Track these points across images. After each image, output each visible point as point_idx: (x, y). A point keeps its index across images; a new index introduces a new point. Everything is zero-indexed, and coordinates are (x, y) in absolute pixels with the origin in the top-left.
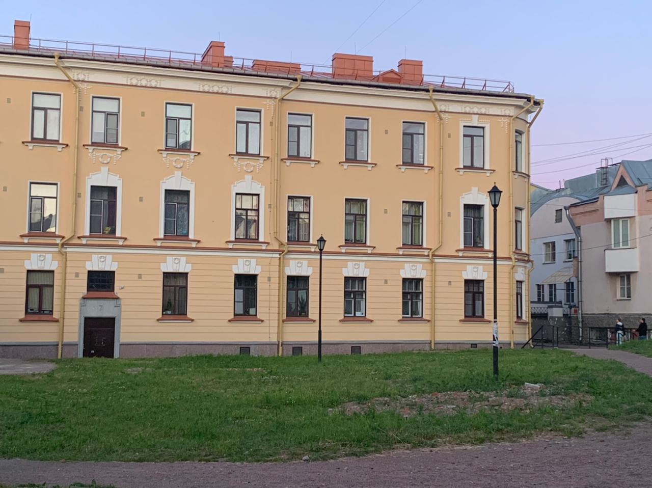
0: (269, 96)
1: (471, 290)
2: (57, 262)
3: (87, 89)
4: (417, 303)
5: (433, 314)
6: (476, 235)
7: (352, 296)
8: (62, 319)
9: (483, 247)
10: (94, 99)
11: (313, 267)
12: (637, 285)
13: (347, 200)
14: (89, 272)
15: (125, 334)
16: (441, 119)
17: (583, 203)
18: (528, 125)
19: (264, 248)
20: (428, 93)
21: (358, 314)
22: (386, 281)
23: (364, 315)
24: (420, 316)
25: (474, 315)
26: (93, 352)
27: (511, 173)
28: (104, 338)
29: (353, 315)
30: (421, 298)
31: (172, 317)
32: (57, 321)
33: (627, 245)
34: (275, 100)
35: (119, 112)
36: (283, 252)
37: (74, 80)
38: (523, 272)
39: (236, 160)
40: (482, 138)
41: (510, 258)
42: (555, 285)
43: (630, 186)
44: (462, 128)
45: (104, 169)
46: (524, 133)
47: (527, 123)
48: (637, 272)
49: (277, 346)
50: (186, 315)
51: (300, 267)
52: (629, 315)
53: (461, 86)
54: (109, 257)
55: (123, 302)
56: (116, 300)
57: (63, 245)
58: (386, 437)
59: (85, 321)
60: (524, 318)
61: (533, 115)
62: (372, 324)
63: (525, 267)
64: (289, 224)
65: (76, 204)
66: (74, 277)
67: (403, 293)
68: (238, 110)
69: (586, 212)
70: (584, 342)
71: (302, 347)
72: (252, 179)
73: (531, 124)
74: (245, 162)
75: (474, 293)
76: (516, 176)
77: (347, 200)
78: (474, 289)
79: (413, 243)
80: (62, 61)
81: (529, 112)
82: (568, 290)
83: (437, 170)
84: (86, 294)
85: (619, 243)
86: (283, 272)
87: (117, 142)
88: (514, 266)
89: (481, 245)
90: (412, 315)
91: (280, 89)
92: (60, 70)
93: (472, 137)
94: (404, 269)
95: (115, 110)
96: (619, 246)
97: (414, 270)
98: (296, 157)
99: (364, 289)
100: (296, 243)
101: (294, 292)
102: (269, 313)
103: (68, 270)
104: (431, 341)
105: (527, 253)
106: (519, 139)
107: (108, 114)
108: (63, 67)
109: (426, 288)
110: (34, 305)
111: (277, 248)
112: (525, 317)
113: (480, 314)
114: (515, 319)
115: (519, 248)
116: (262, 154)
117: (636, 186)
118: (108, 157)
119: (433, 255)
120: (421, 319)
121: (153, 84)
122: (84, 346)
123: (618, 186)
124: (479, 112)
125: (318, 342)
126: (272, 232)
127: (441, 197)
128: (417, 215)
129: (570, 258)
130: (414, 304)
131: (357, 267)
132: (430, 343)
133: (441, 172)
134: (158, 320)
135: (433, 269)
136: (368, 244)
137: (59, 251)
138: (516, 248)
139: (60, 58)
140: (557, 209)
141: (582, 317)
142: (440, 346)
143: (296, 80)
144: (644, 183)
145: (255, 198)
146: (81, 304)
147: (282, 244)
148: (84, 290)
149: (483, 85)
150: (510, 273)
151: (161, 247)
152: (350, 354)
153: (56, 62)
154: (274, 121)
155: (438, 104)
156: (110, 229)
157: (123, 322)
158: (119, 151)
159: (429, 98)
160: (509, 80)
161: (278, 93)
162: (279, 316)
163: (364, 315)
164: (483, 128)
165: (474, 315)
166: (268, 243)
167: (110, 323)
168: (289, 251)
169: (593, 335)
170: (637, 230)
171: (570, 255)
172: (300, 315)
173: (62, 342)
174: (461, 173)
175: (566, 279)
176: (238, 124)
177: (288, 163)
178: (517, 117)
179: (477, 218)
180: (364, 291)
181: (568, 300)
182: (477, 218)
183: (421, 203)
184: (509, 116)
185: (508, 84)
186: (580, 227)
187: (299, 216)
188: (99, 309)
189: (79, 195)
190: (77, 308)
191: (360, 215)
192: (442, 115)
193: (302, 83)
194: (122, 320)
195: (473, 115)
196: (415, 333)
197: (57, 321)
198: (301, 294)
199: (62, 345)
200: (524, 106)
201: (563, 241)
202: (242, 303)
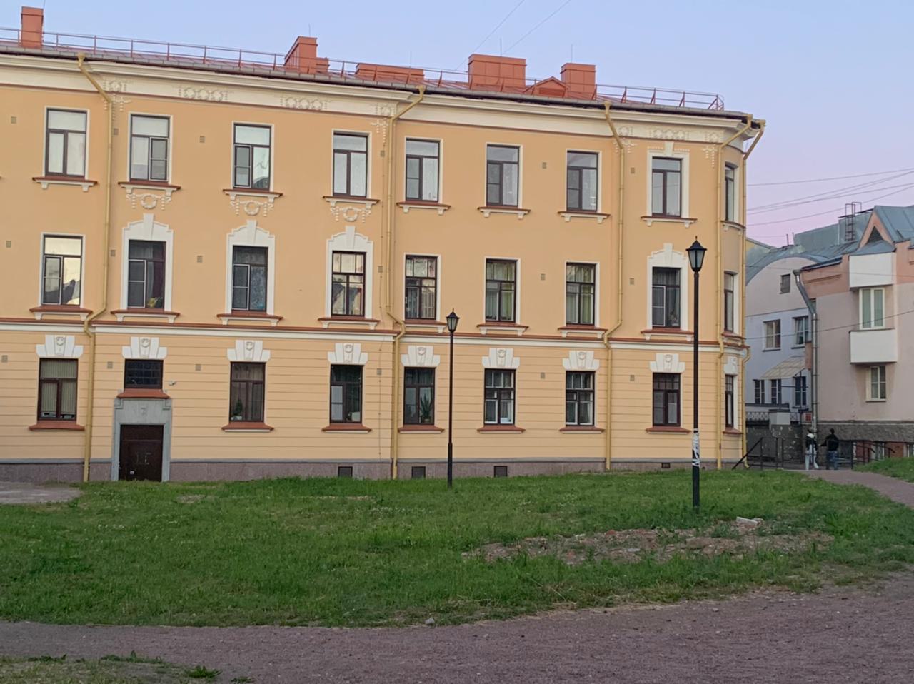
2: (82, 347)
4: (506, 405)
5: (609, 421)
6: (670, 310)
7: (496, 396)
9: (679, 327)
12: (897, 382)
13: (488, 261)
14: (127, 360)
15: (178, 448)
16: (621, 147)
17: (820, 266)
20: (602, 111)
21: (503, 421)
22: (543, 375)
23: (512, 422)
24: (591, 424)
25: (666, 423)
26: (132, 472)
27: (719, 223)
28: (148, 454)
29: (496, 422)
30: (591, 399)
31: (244, 424)
32: (82, 429)
33: (882, 325)
34: (718, 146)
35: (168, 137)
36: (399, 333)
40: (679, 174)
41: (717, 343)
43: (886, 242)
44: (650, 160)
46: (737, 167)
47: (742, 153)
49: (390, 465)
50: (263, 421)
51: (349, 352)
53: (649, 101)
54: (259, 344)
55: (174, 403)
57: (90, 323)
60: (736, 426)
61: (751, 141)
62: (524, 435)
63: (738, 355)
64: (406, 295)
65: (108, 266)
66: (375, 375)
67: (567, 391)
73: (747, 154)
74: (345, 207)
75: (667, 392)
76: (726, 228)
78: (665, 385)
79: (581, 322)
80: (89, 65)
82: (798, 387)
84: (123, 391)
85: (870, 322)
86: (399, 361)
87: (166, 179)
88: (722, 354)
90: (579, 422)
91: (395, 105)
93: (664, 172)
96: (870, 326)
98: (416, 201)
99: (512, 386)
103: (98, 358)
105: (741, 335)
106: (730, 176)
107: (153, 139)
108: (91, 73)
109: (599, 384)
110: (50, 407)
112: (738, 425)
113: (675, 422)
114: (724, 428)
115: (729, 328)
116: (369, 197)
117: (894, 242)
118: (354, 213)
119: (609, 339)
120: (592, 428)
121: (217, 97)
123: (869, 241)
124: (675, 138)
125: (447, 460)
126: (383, 306)
127: (621, 258)
128: (587, 282)
129: (801, 343)
130: (502, 406)
133: (621, 223)
134: (223, 429)
135: (610, 358)
137: (85, 332)
139: (86, 60)
143: (417, 91)
144: (905, 237)
145: (360, 258)
146: (115, 405)
147: (397, 323)
149: (681, 99)
150: (717, 364)
153: (80, 65)
155: (617, 126)
156: (156, 301)
157: (175, 432)
158: (169, 191)
159: (604, 117)
160: (717, 93)
161: (391, 111)
163: (512, 422)
164: (680, 160)
165: (666, 423)
167: (156, 432)
168: (407, 333)
170: (894, 304)
171: (802, 338)
173: (610, 458)
174: (649, 224)
175: (796, 372)
177: (406, 208)
178: (727, 145)
179: (672, 286)
180: (512, 389)
181: (798, 402)
182: (672, 286)
183: (593, 266)
184: (717, 143)
185: (715, 98)
186: (815, 299)
188: (141, 413)
189: (112, 253)
190: (110, 412)
192: (623, 142)
195: (666, 142)
196: (583, 447)
197: (82, 429)
198: (425, 392)
200: (738, 129)
201: (791, 319)
202: (341, 406)
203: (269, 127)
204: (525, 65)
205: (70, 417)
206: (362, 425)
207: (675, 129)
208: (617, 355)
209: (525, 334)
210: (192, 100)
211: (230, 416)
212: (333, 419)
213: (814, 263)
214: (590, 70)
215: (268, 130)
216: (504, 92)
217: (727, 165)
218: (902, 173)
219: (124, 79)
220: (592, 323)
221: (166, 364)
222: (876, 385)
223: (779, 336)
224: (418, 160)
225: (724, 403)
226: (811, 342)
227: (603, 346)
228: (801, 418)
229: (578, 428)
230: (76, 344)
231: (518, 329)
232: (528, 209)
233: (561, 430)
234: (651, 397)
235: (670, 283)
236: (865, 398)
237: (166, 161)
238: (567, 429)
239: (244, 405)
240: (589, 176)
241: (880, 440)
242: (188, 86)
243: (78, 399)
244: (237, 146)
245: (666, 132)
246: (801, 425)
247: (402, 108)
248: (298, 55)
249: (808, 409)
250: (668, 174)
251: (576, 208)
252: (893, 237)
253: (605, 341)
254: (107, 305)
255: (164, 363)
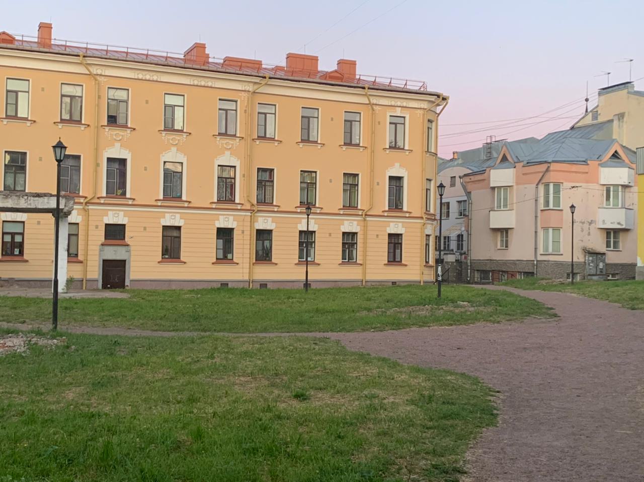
0: (243, 89)
1: (393, 241)
2: (81, 217)
3: (379, 110)
4: (352, 251)
5: (365, 259)
6: (397, 199)
7: (304, 245)
8: (86, 261)
9: (402, 209)
10: (63, 85)
11: (276, 223)
12: (514, 238)
13: (344, 174)
14: (218, 228)
15: (135, 272)
16: (373, 110)
17: (474, 174)
18: (437, 115)
19: (239, 208)
20: (364, 90)
22: (330, 234)
23: (313, 260)
24: (355, 261)
26: (109, 286)
27: (424, 153)
28: (117, 276)
30: (355, 247)
32: (81, 262)
33: (507, 207)
34: (249, 93)
35: (128, 100)
36: (254, 211)
37: (95, 75)
38: (431, 228)
39: (218, 139)
41: (422, 218)
42: (448, 237)
44: (388, 118)
45: (118, 145)
46: (433, 121)
47: (437, 114)
48: (513, 228)
49: (248, 283)
50: (180, 258)
52: (506, 261)
53: (403, 86)
54: (122, 214)
55: (132, 248)
56: (127, 247)
57: (86, 203)
58: (72, 359)
59: (103, 262)
61: (441, 107)
62: (277, 266)
63: (432, 224)
64: (257, 190)
65: (96, 171)
66: (328, 236)
67: (343, 243)
68: (220, 100)
69: (476, 181)
70: (471, 281)
71: (266, 284)
72: (231, 154)
75: (395, 244)
76: (428, 155)
77: (344, 174)
78: (395, 241)
79: (350, 205)
81: (438, 105)
82: (458, 241)
83: (369, 150)
86: (254, 227)
87: (127, 123)
88: (425, 224)
89: (401, 207)
90: (349, 260)
91: (252, 84)
92: (83, 66)
93: (396, 124)
94: (107, 216)
95: (125, 98)
96: (500, 208)
97: (173, 219)
98: (263, 138)
99: (313, 240)
100: (262, 204)
101: (261, 242)
102: (243, 258)
103: (90, 223)
104: (83, 279)
105: (434, 213)
109: (360, 239)
111: (249, 208)
112: (432, 262)
113: (399, 260)
114: (424, 264)
115: (428, 209)
117: (515, 163)
119: (366, 215)
120: (355, 263)
121: (155, 78)
122: (103, 281)
123: (501, 161)
124: (402, 105)
126: (245, 196)
127: (372, 171)
128: (354, 183)
129: (461, 215)
130: (350, 251)
131: (227, 220)
132: (362, 281)
133: (373, 152)
134: (159, 262)
136: (275, 203)
137: (83, 208)
138: (426, 210)
139: (84, 57)
140: (345, 172)
141: (471, 262)
142: (369, 284)
144: (521, 160)
145: (233, 169)
146: (100, 249)
147: (253, 205)
148: (102, 239)
150: (422, 229)
151: (215, 209)
152: (259, 288)
153: (81, 60)
154: (247, 109)
155: (371, 98)
157: (132, 264)
158: (129, 131)
159: (364, 93)
161: (250, 88)
162: (250, 261)
163: (313, 260)
164: (404, 117)
165: (394, 261)
166: (242, 204)
167: (122, 264)
169: (477, 275)
170: (514, 197)
171: (461, 213)
172: (265, 260)
173: (86, 278)
174: (388, 152)
175: (458, 232)
176: (259, 115)
177: (258, 142)
178: (430, 110)
179: (398, 186)
181: (458, 249)
182: (398, 186)
183: (357, 175)
184: (424, 109)
187: (265, 183)
188: (114, 253)
189: (98, 165)
190: (97, 253)
191: (312, 183)
192: (374, 107)
193: (270, 80)
194: (131, 262)
195: (397, 108)
196: (351, 273)
197: (81, 262)
198: (267, 243)
199: (86, 281)
201: (456, 202)
203: (183, 96)
204: (205, 48)
205: (74, 255)
206: (23, 258)
207: (402, 100)
208: (369, 223)
209: (189, 206)
210: (149, 80)
211: (162, 255)
212: (218, 257)
213: (471, 172)
214: (353, 64)
215: (28, 82)
216: (311, 78)
217: (429, 121)
218: (509, 125)
219: (104, 68)
220: (356, 206)
221: (405, 236)
222: (503, 240)
223: (449, 211)
224: (264, 115)
225: (425, 250)
226: (468, 216)
227: (362, 219)
228: (461, 258)
229: (348, 263)
230: (78, 215)
231: (275, 207)
232: (323, 143)
233: (339, 264)
234: (387, 247)
235: (398, 185)
236: (497, 247)
237: (127, 114)
238: (343, 263)
239: (169, 248)
240: (356, 126)
241: (504, 270)
242: (139, 72)
243: (79, 245)
244: (166, 106)
245: (208, 82)
246: (461, 262)
247: (256, 87)
248: (195, 54)
249: (465, 253)
250: (398, 125)
251: (349, 143)
252: (514, 159)
253: (364, 216)
254: (95, 194)
255: (126, 226)
